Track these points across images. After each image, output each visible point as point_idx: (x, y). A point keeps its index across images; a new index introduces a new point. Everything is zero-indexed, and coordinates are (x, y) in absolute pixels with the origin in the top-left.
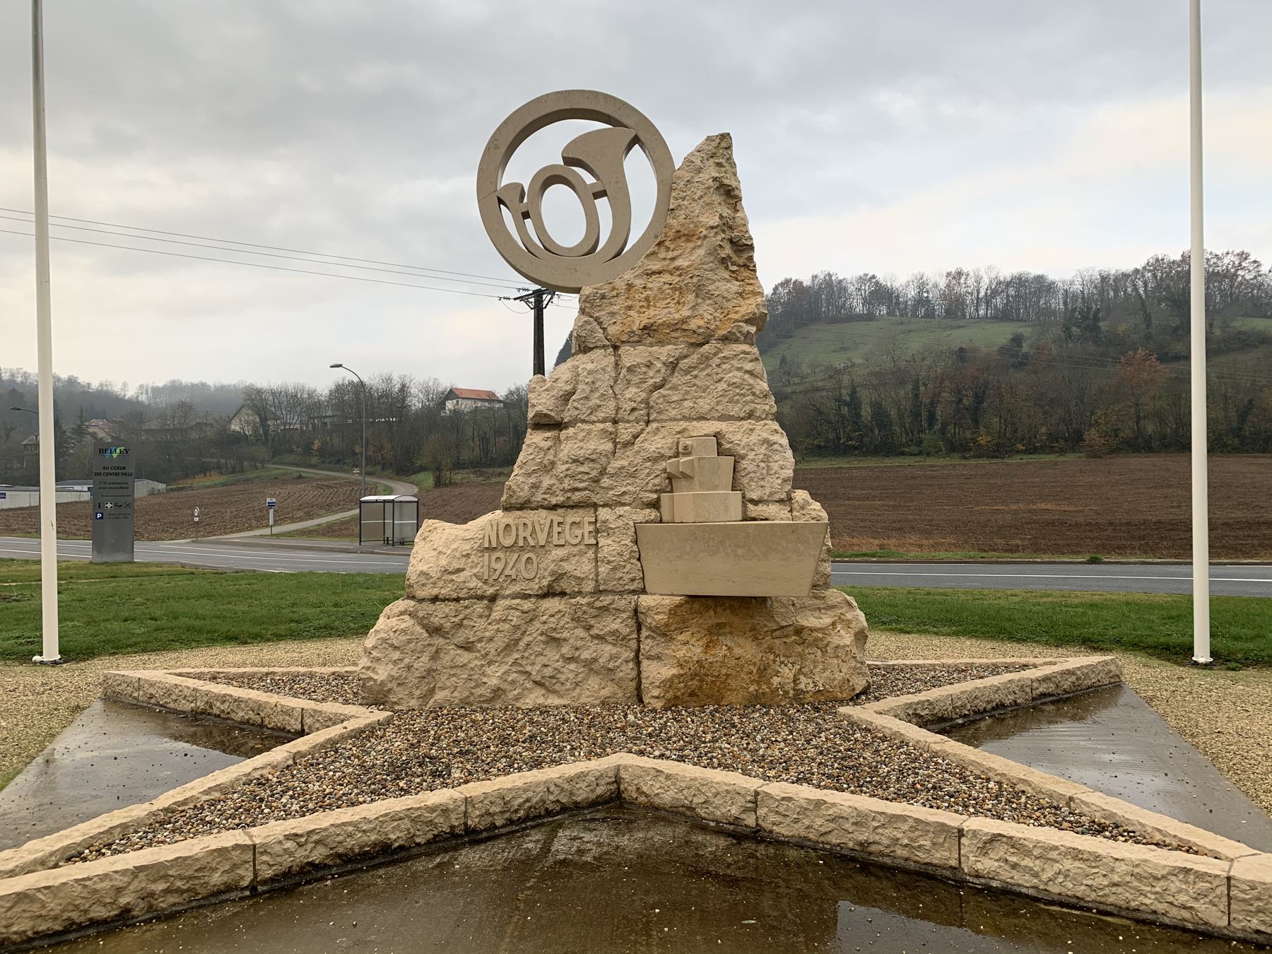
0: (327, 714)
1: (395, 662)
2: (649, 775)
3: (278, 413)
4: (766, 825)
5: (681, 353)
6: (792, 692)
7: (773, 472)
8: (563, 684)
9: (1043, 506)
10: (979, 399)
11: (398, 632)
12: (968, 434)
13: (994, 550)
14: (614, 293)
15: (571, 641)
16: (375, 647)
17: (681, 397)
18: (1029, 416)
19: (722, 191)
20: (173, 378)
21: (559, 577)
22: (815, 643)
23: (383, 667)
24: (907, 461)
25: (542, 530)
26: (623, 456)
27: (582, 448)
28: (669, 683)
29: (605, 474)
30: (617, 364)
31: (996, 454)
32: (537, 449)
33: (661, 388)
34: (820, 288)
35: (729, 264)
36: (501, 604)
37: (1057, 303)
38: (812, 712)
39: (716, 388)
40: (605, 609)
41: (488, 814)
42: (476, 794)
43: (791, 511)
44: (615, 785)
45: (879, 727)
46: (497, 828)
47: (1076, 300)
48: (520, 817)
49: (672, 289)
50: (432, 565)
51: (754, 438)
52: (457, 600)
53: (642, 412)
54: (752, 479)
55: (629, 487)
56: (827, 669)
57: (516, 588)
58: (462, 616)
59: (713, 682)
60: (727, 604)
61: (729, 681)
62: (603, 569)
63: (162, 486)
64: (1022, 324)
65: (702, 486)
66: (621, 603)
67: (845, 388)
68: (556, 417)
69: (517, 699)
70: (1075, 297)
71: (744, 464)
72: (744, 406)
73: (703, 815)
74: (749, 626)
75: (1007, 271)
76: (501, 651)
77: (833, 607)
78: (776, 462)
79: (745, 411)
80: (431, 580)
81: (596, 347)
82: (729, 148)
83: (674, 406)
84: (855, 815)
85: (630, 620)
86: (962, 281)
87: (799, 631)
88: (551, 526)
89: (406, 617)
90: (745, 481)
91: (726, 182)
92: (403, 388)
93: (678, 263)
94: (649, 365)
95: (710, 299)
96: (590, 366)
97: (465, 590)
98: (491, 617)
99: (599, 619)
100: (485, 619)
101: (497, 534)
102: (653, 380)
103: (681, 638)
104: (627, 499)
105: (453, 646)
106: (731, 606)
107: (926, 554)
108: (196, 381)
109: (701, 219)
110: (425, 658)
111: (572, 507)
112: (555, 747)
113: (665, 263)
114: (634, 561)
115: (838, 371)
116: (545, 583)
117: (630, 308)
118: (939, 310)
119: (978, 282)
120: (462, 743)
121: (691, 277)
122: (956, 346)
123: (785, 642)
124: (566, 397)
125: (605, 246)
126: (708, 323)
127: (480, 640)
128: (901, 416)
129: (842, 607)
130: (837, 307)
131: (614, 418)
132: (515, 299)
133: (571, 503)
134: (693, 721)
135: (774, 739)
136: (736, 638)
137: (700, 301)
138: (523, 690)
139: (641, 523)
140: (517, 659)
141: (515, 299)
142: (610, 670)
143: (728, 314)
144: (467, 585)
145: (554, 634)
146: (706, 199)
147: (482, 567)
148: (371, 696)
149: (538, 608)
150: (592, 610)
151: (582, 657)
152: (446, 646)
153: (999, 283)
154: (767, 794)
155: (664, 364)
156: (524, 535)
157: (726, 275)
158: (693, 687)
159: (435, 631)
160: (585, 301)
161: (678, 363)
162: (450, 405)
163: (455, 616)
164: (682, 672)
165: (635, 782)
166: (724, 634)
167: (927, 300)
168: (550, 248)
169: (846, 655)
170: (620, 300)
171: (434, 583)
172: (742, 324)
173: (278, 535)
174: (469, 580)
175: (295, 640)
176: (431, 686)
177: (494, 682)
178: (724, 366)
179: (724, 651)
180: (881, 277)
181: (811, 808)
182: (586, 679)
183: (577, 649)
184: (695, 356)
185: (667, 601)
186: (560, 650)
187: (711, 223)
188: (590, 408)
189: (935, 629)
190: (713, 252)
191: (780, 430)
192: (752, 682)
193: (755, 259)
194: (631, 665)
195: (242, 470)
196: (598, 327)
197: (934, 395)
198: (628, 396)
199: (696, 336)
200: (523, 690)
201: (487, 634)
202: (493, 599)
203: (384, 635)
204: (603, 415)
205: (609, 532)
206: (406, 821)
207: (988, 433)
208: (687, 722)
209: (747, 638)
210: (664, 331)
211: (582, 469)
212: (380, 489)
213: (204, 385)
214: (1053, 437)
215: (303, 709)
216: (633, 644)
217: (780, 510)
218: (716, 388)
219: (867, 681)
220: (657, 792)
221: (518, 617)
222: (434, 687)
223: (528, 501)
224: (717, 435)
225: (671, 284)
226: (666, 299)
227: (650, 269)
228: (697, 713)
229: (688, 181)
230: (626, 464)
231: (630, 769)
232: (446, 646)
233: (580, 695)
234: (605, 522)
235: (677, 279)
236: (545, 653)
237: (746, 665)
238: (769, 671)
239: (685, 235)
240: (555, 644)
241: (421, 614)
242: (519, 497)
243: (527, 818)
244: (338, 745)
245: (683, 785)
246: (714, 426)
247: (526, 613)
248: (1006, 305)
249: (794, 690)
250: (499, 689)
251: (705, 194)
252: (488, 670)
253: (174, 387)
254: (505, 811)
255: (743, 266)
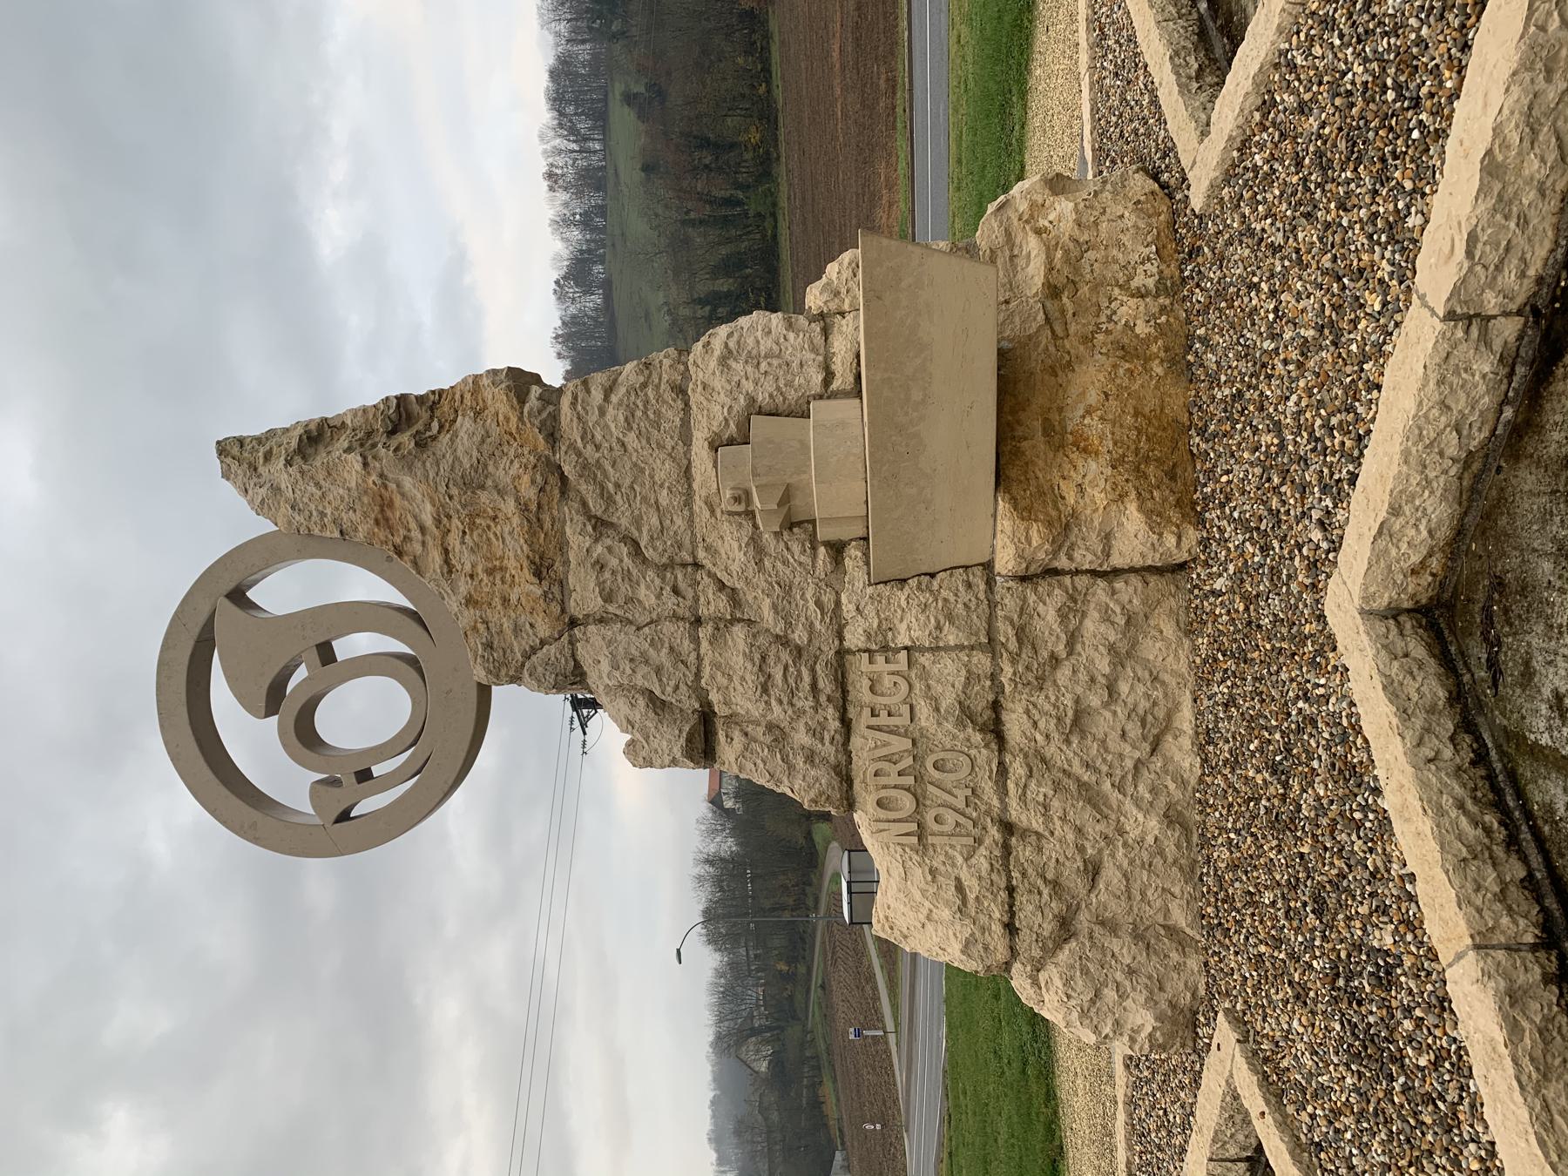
0: (1222, 1122)
1: (1122, 996)
2: (1386, 551)
3: (744, 1014)
4: (1522, 291)
5: (578, 512)
6: (1161, 300)
7: (775, 347)
8: (1155, 704)
9: (836, 54)
10: (705, 143)
11: (1070, 992)
12: (748, 156)
13: (894, 108)
14: (481, 627)
15: (1079, 690)
16: (1096, 1030)
17: (652, 511)
18: (724, 79)
19: (310, 451)
20: (706, 1141)
21: (966, 714)
22: (1073, 262)
23: (1131, 1016)
24: (783, 233)
25: (886, 744)
26: (755, 607)
27: (743, 678)
28: (1156, 519)
29: (786, 637)
30: (601, 621)
31: (772, 119)
32: (748, 754)
33: (638, 545)
34: (572, 349)
35: (428, 434)
36: (1015, 813)
37: (584, 52)
38: (1200, 260)
39: (636, 451)
40: (1021, 633)
41: (1502, 896)
42: (1462, 923)
43: (842, 314)
44: (1402, 618)
45: (1241, 120)
46: (1530, 875)
47: (579, 28)
48: (1501, 823)
49: (472, 531)
50: (951, 933)
51: (718, 383)
52: (1011, 890)
53: (680, 577)
54: (789, 384)
55: (809, 595)
56: (1119, 241)
57: (988, 788)
58: (1040, 882)
59: (1148, 439)
60: (1010, 418)
61: (1147, 410)
62: (951, 637)
63: (838, 1156)
64: (610, 95)
65: (803, 468)
66: (1009, 604)
67: (695, 313)
68: (692, 722)
69: (1183, 783)
70: (574, 31)
71: (762, 398)
72: (665, 402)
73: (1485, 433)
74: (1046, 377)
75: (543, 115)
76: (1100, 812)
77: (1008, 233)
78: (758, 342)
79: (674, 401)
80: (978, 934)
81: (573, 655)
82: (241, 441)
83: (668, 522)
84: (1527, 76)
85: (1040, 589)
86: (559, 172)
87: (1052, 291)
88: (878, 729)
89: (1043, 976)
90: (792, 395)
91: (294, 444)
92: (709, 861)
93: (428, 521)
94: (600, 566)
95: (486, 466)
96: (605, 666)
97: (995, 877)
98: (1041, 830)
99: (1039, 642)
100: (1044, 841)
101: (894, 821)
102: (626, 559)
103: (1071, 499)
104: (828, 598)
105: (1093, 895)
106: (1013, 412)
107: (901, 196)
108: (709, 1112)
109: (353, 485)
110: (1115, 945)
111: (845, 692)
112: (1300, 730)
113: (431, 543)
114: (935, 584)
115: (674, 322)
116: (977, 738)
117: (505, 601)
118: (596, 199)
119: (560, 152)
120: (1292, 904)
121: (451, 498)
122: (639, 176)
123: (1074, 315)
124: (657, 705)
125: (402, 641)
126: (526, 468)
127: (1081, 849)
128: (729, 240)
129: (1008, 218)
130: (595, 327)
131: (691, 624)
132: (585, 733)
133: (838, 695)
134: (1228, 472)
135: (1271, 316)
136: (1069, 401)
137: (489, 483)
138: (1167, 772)
139: (869, 574)
140: (1113, 785)
141: (585, 733)
142: (1128, 622)
143: (511, 434)
144: (984, 874)
145: (1068, 722)
146: (320, 477)
147: (952, 846)
148: (1180, 1033)
149: (1021, 750)
150: (1024, 656)
151: (1107, 670)
152: (1093, 908)
153: (561, 125)
154: (1455, 292)
155: (596, 541)
156: (894, 775)
157: (445, 439)
158: (1160, 473)
159: (1065, 928)
160: (497, 677)
161: (595, 517)
162: (729, 804)
163: (1040, 893)
164: (1133, 495)
165: (1399, 578)
166: (1062, 422)
167: (585, 214)
168: (414, 735)
169: (1092, 207)
170: (493, 617)
171: (983, 930)
172: (526, 410)
173: (897, 1024)
174: (976, 870)
175: (1053, 1073)
176: (1163, 932)
177: (1154, 825)
178: (598, 437)
179: (1093, 422)
180: (555, 275)
181: (1497, 186)
182: (1146, 663)
183: (1093, 680)
184: (583, 487)
185: (1005, 523)
186: (1095, 710)
187: (358, 467)
188: (675, 666)
189: (1017, 128)
190: (407, 461)
191: (704, 339)
192: (1148, 370)
193: (422, 392)
194: (1119, 585)
195: (817, 1057)
196: (540, 654)
197: (700, 199)
198: (653, 600)
199: (548, 488)
200: (1167, 772)
201: (1071, 837)
202: (1008, 828)
203: (1075, 1015)
204: (686, 643)
205: (886, 628)
206: (1550, 1093)
207: (747, 131)
208: (1229, 482)
209: (1069, 381)
210: (542, 540)
211: (778, 677)
212: (834, 888)
213: (713, 1103)
214: (750, 49)
215: (1211, 1160)
216: (1082, 581)
217: (841, 333)
218: (636, 451)
219: (1137, 171)
220: (1425, 533)
221: (1039, 784)
222: (1163, 926)
223: (837, 769)
224: (714, 446)
225: (464, 532)
226: (488, 539)
227: (441, 567)
228: (1208, 465)
229: (293, 508)
230: (768, 601)
231: (1372, 589)
232: (1093, 908)
233: (1174, 673)
234: (869, 637)
235: (455, 521)
236: (1101, 736)
237: (1118, 381)
238: (1126, 340)
239: (382, 511)
240: (1085, 720)
241: (1037, 953)
242: (829, 784)
243: (1499, 805)
244: (1303, 1137)
245: (1415, 479)
246: (700, 451)
247: (1031, 771)
248: (587, 116)
249: (1157, 296)
250: (1166, 815)
251: (312, 478)
252: (1133, 834)
253: (717, 1139)
254: (1491, 857)
255: (432, 411)
